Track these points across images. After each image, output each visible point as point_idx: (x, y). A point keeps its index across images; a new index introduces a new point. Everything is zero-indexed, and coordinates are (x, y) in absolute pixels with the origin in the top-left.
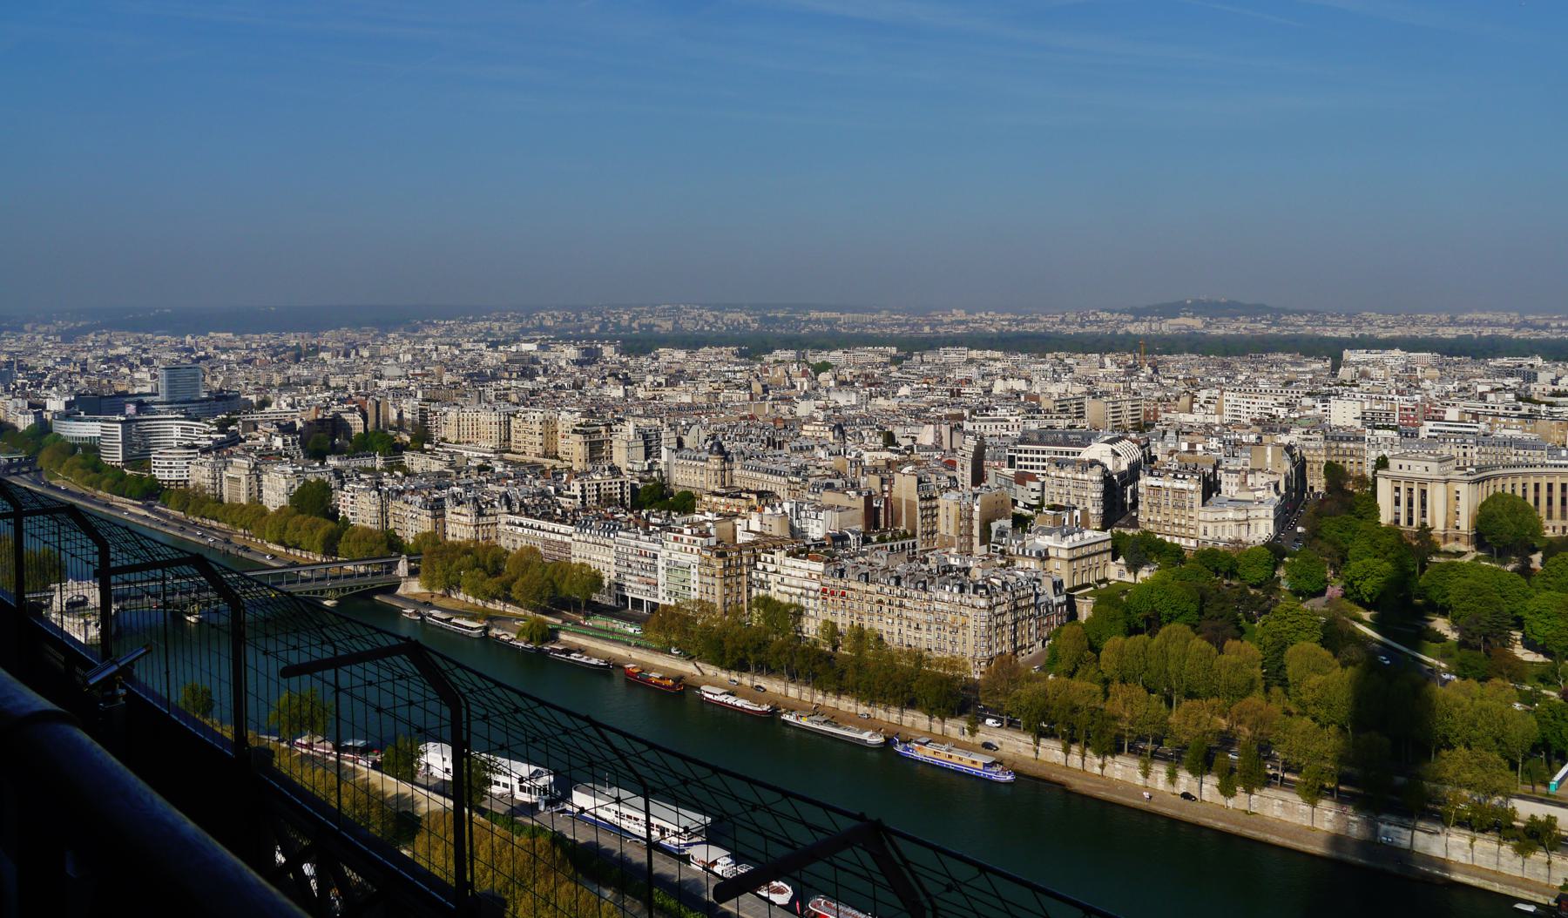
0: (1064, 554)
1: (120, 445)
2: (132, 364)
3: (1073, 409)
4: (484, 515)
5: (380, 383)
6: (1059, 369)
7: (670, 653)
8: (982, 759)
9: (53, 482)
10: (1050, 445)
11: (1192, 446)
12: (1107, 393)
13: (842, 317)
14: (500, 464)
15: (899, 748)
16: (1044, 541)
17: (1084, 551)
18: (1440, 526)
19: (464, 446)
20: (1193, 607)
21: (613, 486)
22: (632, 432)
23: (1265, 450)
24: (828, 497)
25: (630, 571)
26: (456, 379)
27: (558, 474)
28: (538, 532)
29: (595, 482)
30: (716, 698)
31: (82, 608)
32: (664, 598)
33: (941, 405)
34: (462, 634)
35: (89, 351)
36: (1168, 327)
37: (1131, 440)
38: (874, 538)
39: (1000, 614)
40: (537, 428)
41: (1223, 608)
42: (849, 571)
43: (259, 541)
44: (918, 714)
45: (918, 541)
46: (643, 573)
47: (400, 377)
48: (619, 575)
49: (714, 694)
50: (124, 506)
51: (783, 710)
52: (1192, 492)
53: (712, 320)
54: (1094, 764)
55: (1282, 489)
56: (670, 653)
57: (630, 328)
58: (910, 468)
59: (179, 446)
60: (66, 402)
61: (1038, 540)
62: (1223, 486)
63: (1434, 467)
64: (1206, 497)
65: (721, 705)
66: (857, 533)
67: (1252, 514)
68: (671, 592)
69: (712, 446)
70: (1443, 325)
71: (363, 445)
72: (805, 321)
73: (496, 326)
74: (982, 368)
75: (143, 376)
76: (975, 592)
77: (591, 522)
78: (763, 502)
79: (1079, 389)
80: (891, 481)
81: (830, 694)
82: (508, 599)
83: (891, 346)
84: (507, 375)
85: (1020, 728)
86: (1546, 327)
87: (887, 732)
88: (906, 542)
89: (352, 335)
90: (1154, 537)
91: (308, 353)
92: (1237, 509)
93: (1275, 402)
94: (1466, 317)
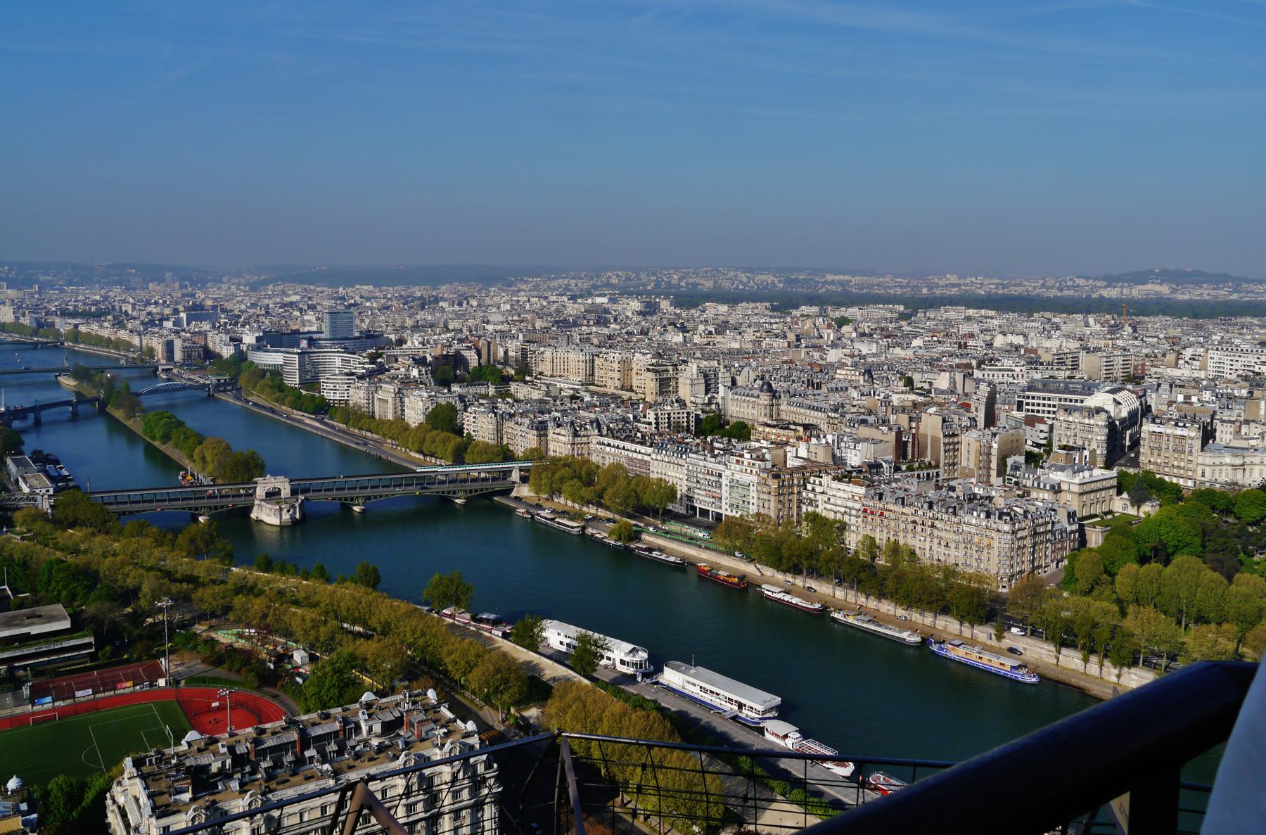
0: (1076, 489)
2: (302, 309)
3: (1069, 362)
4: (579, 436)
5: (487, 327)
7: (734, 556)
8: (1009, 662)
11: (1187, 397)
12: (1099, 349)
14: (588, 394)
15: (935, 648)
16: (1057, 476)
17: (1093, 486)
19: (558, 379)
20: (1198, 541)
21: (681, 416)
22: (695, 371)
23: (1259, 404)
24: (864, 431)
25: (699, 486)
26: (546, 325)
27: (635, 404)
28: (623, 451)
30: (774, 595)
31: (277, 497)
32: (727, 510)
34: (564, 531)
35: (270, 298)
36: (1137, 292)
37: (1129, 390)
38: (904, 467)
39: (1021, 538)
40: (616, 366)
41: (1225, 543)
42: (887, 495)
43: (403, 449)
45: (941, 471)
46: (710, 489)
47: (502, 323)
48: (689, 489)
50: (302, 418)
51: (832, 609)
52: (1192, 438)
53: (745, 280)
56: (734, 556)
59: (341, 374)
60: (257, 337)
62: (1218, 434)
64: (1205, 443)
65: (778, 601)
66: (890, 463)
67: (1248, 460)
68: (733, 505)
71: (478, 376)
76: (1000, 518)
77: (667, 445)
78: (808, 433)
79: (1073, 345)
80: (919, 419)
81: (872, 598)
84: (585, 322)
85: (1042, 637)
87: (922, 633)
88: (931, 471)
89: (462, 289)
90: (1155, 477)
91: (430, 303)
92: (1235, 456)
93: (1258, 361)
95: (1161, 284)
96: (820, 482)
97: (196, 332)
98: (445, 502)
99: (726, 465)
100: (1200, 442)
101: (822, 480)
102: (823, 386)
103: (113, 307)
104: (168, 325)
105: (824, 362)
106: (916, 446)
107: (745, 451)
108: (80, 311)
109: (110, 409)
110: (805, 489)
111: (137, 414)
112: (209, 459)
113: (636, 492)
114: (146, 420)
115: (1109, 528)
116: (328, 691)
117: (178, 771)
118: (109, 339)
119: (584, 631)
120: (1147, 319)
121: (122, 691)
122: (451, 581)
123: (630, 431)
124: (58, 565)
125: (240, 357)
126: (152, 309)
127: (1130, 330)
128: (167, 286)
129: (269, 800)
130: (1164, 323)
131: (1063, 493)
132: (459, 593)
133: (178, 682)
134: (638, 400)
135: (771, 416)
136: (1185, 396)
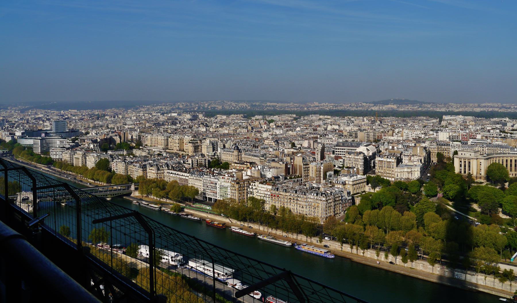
0: (351, 183)
1: (40, 147)
2: (44, 120)
3: (354, 135)
4: (160, 170)
5: (125, 126)
6: (349, 122)
7: (221, 216)
8: (324, 251)
9: (17, 159)
10: (346, 147)
11: (393, 147)
12: (365, 130)
13: (278, 105)
14: (165, 153)
15: (297, 247)
16: (344, 179)
17: (358, 182)
18: (475, 174)
19: (153, 147)
20: (393, 200)
21: (202, 160)
22: (208, 143)
23: (417, 149)
24: (273, 164)
25: (208, 188)
26: (150, 125)
27: (184, 156)
28: (177, 176)
29: (196, 159)
30: (236, 230)
31: (27, 201)
32: (219, 197)
33: (310, 134)
34: (152, 209)
35: (29, 116)
36: (385, 108)
37: (373, 145)
38: (288, 178)
39: (330, 203)
40: (177, 141)
41: (403, 201)
42: (280, 189)
43: (85, 179)
44: (303, 236)
45: (303, 179)
46: (212, 189)
47: (132, 125)
48: (204, 190)
49: (235, 229)
50: (41, 167)
51: (258, 234)
52: (393, 162)
53: (235, 106)
54: (361, 252)
55: (423, 161)
56: (221, 216)
57: (208, 108)
58: (300, 154)
59: (59, 147)
60: (22, 133)
62: (403, 161)
63: (473, 154)
64: (398, 164)
65: (238, 233)
66: (283, 176)
67: (413, 170)
68: (221, 195)
69: (235, 147)
70: (476, 107)
71: (120, 147)
72: (265, 106)
73: (164, 108)
74: (324, 121)
75: (47, 124)
76: (321, 195)
77: (195, 172)
78: (252, 166)
79: (356, 128)
80: (294, 159)
81: (274, 229)
82: (167, 198)
83: (294, 114)
84: (167, 124)
85: (336, 240)
86: (510, 108)
87: (292, 241)
88: (299, 179)
89: (116, 111)
90: (381, 177)
91: (101, 117)
92: (408, 168)
93: (420, 133)
94: (483, 105)
127: (379, 123)
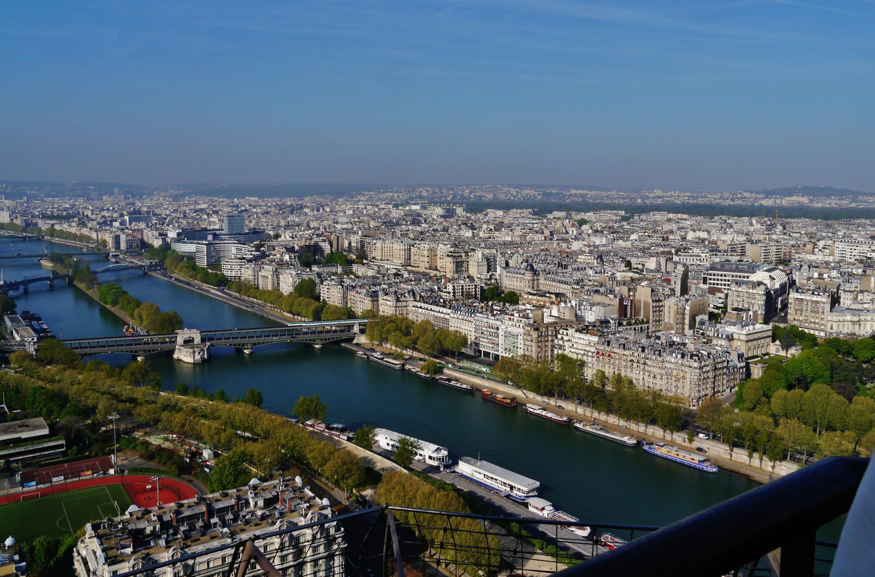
0: (743, 338)
2: (209, 213)
3: (739, 250)
4: (400, 301)
5: (337, 226)
7: (507, 384)
8: (698, 458)
11: (821, 275)
12: (760, 241)
14: (406, 272)
15: (646, 448)
16: (730, 329)
17: (756, 336)
19: (385, 262)
20: (828, 374)
21: (471, 287)
22: (480, 257)
23: (870, 279)
24: (597, 298)
25: (483, 336)
26: (377, 224)
27: (439, 279)
28: (431, 312)
30: (535, 411)
31: (191, 343)
32: (502, 352)
34: (390, 367)
35: (187, 206)
36: (786, 202)
37: (780, 270)
38: (625, 323)
39: (706, 372)
40: (426, 253)
41: (846, 375)
42: (613, 342)
43: (279, 311)
45: (650, 325)
46: (491, 338)
47: (347, 223)
48: (476, 338)
50: (209, 289)
51: (575, 421)
52: (824, 303)
53: (515, 193)
56: (507, 384)
59: (236, 258)
60: (177, 233)
61: (727, 329)
62: (842, 300)
64: (833, 306)
65: (538, 415)
66: (615, 320)
67: (862, 318)
68: (506, 349)
69: (527, 267)
71: (331, 260)
76: (691, 358)
77: (461, 307)
78: (559, 299)
79: (742, 238)
80: (635, 290)
81: (603, 413)
84: (404, 223)
85: (720, 440)
87: (637, 437)
88: (643, 326)
89: (319, 199)
90: (798, 329)
91: (297, 209)
92: (853, 315)
93: (869, 249)
95: (802, 196)
96: (567, 333)
97: (136, 230)
98: (307, 347)
99: (502, 322)
100: (829, 305)
101: (568, 332)
102: (569, 266)
103: (78, 212)
104: (116, 224)
105: (569, 250)
106: (633, 308)
107: (515, 312)
108: (55, 215)
109: (76, 283)
110: (557, 338)
111: (95, 286)
112: (144, 317)
113: (439, 340)
114: (101, 290)
115: (767, 365)
116: (227, 477)
117: (123, 533)
118: (75, 234)
119: (403, 436)
120: (793, 220)
121: (84, 478)
122: (312, 401)
123: (436, 298)
124: (40, 390)
125: (166, 247)
126: (105, 213)
127: (781, 228)
128: (115, 197)
129: (186, 553)
130: (805, 223)
131: (735, 341)
132: (318, 409)
133: (123, 471)
134: (441, 276)
135: (533, 288)
136: (819, 274)
